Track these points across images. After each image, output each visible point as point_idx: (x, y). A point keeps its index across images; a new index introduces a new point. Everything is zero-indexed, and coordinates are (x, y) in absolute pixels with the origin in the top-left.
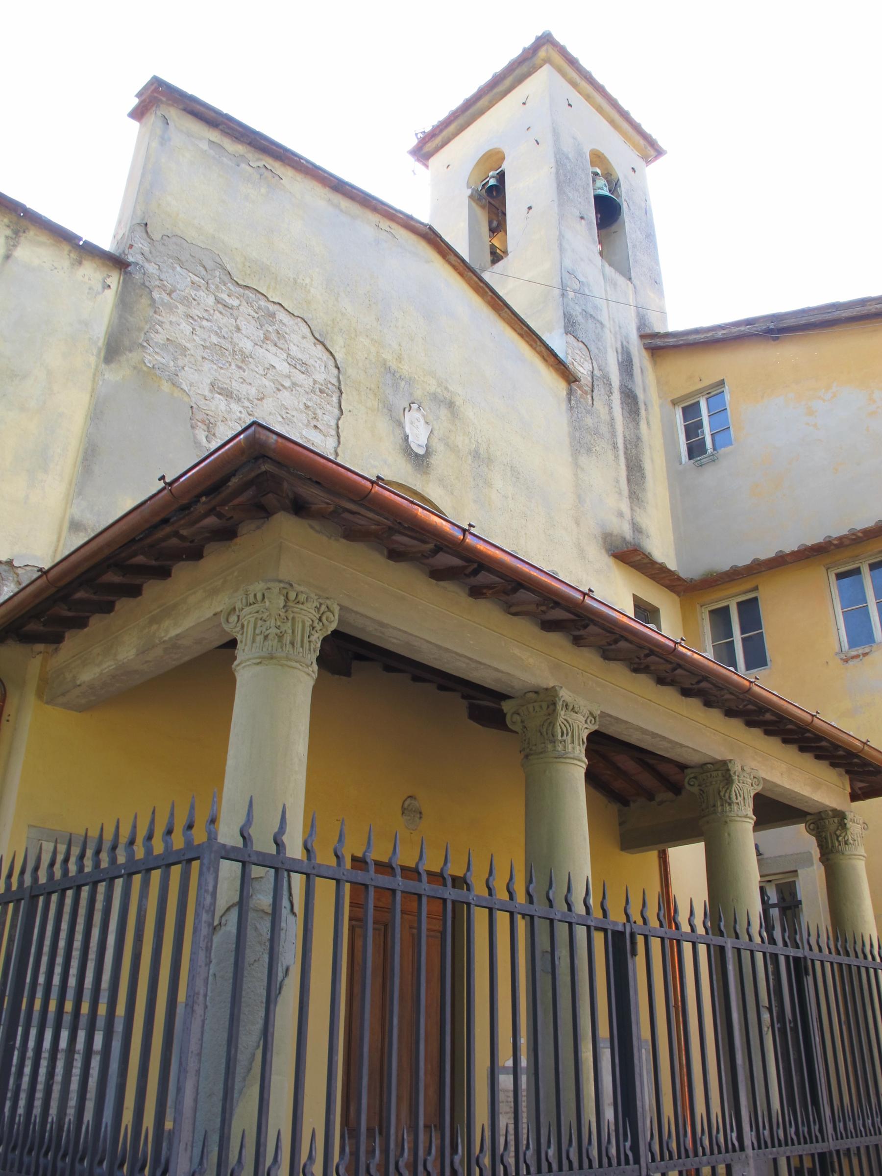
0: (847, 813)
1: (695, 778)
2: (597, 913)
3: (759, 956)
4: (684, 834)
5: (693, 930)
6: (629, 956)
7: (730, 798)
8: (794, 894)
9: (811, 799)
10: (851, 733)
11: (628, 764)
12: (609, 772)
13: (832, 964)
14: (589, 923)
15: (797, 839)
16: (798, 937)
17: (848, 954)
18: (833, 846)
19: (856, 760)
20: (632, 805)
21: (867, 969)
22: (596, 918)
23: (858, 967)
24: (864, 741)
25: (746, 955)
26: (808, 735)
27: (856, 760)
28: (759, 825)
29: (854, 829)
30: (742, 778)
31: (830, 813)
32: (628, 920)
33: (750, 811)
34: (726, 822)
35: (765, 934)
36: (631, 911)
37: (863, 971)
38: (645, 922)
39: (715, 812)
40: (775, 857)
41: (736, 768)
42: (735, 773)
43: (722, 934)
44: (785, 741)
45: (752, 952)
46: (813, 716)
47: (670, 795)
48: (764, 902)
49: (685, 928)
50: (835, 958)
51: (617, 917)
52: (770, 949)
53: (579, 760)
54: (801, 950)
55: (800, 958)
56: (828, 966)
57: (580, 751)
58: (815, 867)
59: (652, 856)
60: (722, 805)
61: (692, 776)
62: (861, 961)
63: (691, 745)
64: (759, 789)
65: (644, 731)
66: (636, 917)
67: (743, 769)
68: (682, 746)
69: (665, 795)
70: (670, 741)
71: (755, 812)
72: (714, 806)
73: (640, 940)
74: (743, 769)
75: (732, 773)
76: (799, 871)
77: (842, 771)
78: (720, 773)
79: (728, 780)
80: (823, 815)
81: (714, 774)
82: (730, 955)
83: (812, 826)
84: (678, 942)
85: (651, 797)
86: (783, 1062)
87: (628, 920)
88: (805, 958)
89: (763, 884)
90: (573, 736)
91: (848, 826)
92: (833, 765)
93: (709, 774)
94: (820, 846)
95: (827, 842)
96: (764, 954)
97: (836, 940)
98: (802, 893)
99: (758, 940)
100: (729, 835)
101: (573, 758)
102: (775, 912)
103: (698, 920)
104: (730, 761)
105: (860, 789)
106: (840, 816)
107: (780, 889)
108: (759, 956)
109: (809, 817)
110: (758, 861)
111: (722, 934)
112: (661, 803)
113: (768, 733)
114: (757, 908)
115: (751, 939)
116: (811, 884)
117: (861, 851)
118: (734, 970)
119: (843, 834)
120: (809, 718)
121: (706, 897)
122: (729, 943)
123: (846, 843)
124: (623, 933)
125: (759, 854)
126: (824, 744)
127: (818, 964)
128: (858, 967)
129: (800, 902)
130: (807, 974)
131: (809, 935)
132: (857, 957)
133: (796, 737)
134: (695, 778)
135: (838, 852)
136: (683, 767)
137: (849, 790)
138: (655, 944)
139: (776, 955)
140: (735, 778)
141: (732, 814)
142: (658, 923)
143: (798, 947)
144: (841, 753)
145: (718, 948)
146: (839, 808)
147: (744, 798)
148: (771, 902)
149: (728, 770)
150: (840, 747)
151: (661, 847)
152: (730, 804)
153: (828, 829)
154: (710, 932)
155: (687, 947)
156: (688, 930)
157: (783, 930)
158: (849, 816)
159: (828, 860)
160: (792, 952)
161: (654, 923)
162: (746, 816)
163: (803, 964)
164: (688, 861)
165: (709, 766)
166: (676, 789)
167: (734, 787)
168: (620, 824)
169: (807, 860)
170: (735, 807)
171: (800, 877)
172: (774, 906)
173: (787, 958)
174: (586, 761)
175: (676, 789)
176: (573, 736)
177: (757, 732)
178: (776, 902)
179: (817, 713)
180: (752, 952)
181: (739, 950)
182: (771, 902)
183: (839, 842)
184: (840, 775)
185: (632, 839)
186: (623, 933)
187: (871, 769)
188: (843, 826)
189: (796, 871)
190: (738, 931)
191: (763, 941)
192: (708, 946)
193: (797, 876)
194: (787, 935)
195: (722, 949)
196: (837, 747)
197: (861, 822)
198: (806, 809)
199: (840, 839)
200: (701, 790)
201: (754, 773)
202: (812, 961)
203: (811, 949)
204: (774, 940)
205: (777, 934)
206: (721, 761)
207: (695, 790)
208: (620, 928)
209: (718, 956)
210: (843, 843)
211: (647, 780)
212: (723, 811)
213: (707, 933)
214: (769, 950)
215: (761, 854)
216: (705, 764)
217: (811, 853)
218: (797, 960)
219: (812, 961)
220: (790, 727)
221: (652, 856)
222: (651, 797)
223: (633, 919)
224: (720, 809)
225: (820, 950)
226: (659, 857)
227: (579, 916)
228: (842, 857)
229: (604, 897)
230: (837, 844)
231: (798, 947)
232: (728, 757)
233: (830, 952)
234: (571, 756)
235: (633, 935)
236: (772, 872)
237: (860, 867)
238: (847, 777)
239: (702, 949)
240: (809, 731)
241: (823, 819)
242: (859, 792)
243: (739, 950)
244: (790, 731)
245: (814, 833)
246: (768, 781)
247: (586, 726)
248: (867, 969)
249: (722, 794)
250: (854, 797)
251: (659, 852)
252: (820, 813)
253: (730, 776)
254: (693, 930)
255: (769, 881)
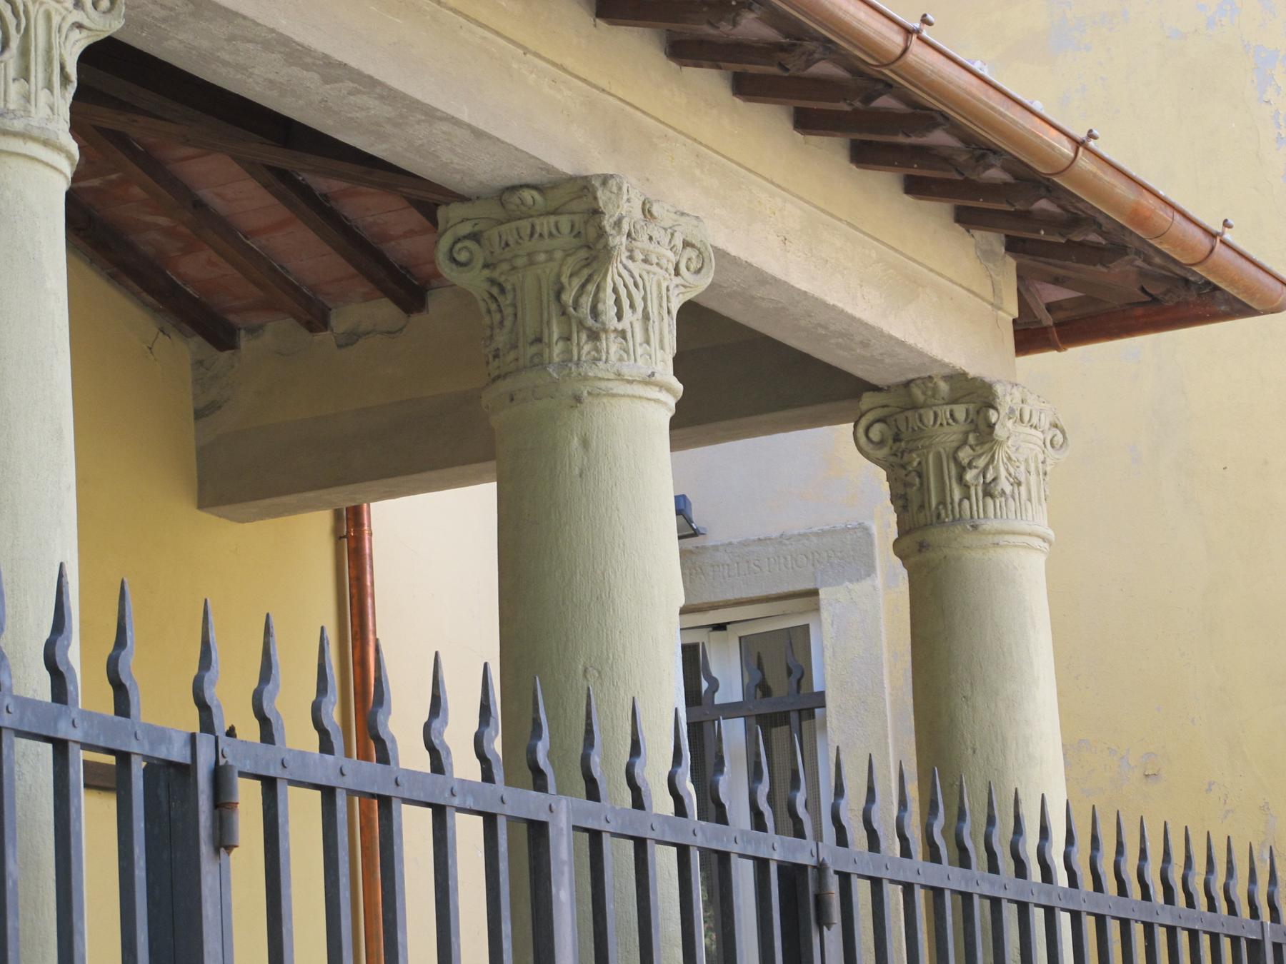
0: (999, 389)
1: (475, 237)
2: (91, 693)
3: (664, 862)
4: (425, 448)
5: (438, 765)
6: (205, 849)
7: (595, 313)
8: (799, 672)
9: (880, 334)
10: (1038, 106)
11: (228, 183)
12: (163, 221)
13: (908, 889)
14: (63, 731)
15: (822, 476)
16: (800, 798)
17: (963, 860)
18: (942, 502)
19: (1043, 204)
20: (244, 341)
21: (1023, 908)
22: (87, 715)
23: (996, 903)
24: (1081, 134)
25: (619, 857)
26: (884, 102)
27: (1043, 204)
28: (691, 423)
29: (1019, 443)
30: (642, 243)
31: (944, 387)
32: (207, 724)
33: (664, 366)
34: (578, 399)
35: (688, 788)
36: (216, 693)
37: (1010, 915)
38: (267, 734)
39: (539, 363)
40: (745, 544)
41: (622, 207)
42: (618, 223)
43: (539, 780)
44: (806, 122)
45: (640, 845)
46: (908, 32)
47: (385, 311)
48: (693, 696)
49: (411, 756)
50: (921, 871)
51: (165, 717)
52: (703, 835)
53: (46, 143)
54: (809, 842)
55: (803, 868)
56: (894, 896)
57: (53, 109)
58: (879, 580)
59: (313, 530)
60: (568, 339)
61: (466, 228)
62: (1005, 884)
63: (465, 117)
64: (697, 286)
65: (296, 53)
66: (234, 709)
67: (647, 212)
68: (431, 114)
69: (368, 312)
70: (391, 96)
71: (681, 366)
72: (539, 340)
73: (248, 796)
74: (647, 212)
75: (607, 223)
76: (821, 592)
77: (995, 241)
78: (564, 221)
79: (593, 250)
80: (917, 392)
81: (545, 224)
82: (565, 853)
83: (875, 433)
84: (385, 802)
85: (314, 316)
86: (706, 879)
87: (207, 724)
88: (821, 868)
89: (692, 638)
90: (24, 52)
91: (999, 432)
92: (967, 218)
93: (525, 225)
94: (901, 500)
95: (924, 488)
96: (683, 851)
97: (930, 809)
98: (829, 669)
99: (662, 803)
100: (585, 443)
101: (24, 136)
102: (733, 733)
103: (459, 733)
104: (605, 180)
105: (1050, 307)
106: (977, 397)
107: (755, 654)
108: (664, 862)
109: (868, 400)
110: (684, 554)
111: (539, 780)
112: (351, 338)
113: (745, 87)
114: (663, 702)
115: (638, 803)
116: (862, 642)
117: (1037, 519)
118: (578, 901)
119: (981, 463)
120: (894, 40)
121: (492, 653)
122: (564, 814)
123: (988, 493)
124: (185, 771)
125: (688, 531)
126: (939, 138)
127: (862, 891)
128: (996, 903)
129: (820, 699)
130: (823, 920)
131: (839, 791)
132: (993, 868)
133: (844, 107)
134: (475, 237)
135: (958, 520)
136: (428, 198)
137: (1012, 309)
138: (302, 810)
139: (724, 858)
140: (619, 241)
141: (600, 370)
142: (315, 736)
143: (800, 834)
144: (995, 174)
145: (524, 827)
146: (972, 372)
147: (646, 317)
148: (719, 699)
149: (596, 212)
150: (996, 151)
151: (344, 497)
152: (594, 336)
153: (932, 447)
154: (498, 773)
155: (415, 826)
156: (422, 763)
157: (755, 775)
158: (1007, 398)
159: (922, 547)
160: (779, 848)
161: (299, 735)
162: (649, 380)
163: (812, 888)
164: (436, 552)
165: (527, 195)
166: (409, 289)
167: (615, 275)
168: (199, 414)
169: (850, 555)
170: (612, 346)
171: (825, 614)
172: (730, 710)
173: (761, 865)
174: (73, 147)
175: (409, 289)
176: (24, 52)
177: (708, 82)
178: (737, 697)
179: (925, 20)
180: (640, 845)
181: (595, 837)
182: (719, 699)
183: (966, 487)
184: (986, 255)
185: (235, 476)
186: (185, 771)
187: (1093, 237)
188: (982, 432)
189: (814, 593)
190: (597, 772)
191: (680, 810)
192: (490, 821)
193: (816, 609)
194: (763, 789)
195: (537, 831)
196: (983, 151)
197: (1045, 423)
198: (859, 371)
199: (969, 476)
200: (493, 282)
201: (685, 229)
202: (845, 878)
203: (842, 840)
204: (720, 807)
205: (733, 786)
206: (572, 179)
207: (473, 280)
208: (178, 753)
209: (524, 855)
210: (976, 492)
211: (304, 253)
212: (567, 359)
213: (488, 776)
214: (700, 841)
215: (696, 533)
216: (514, 189)
217: (866, 531)
218: (792, 875)
219: (845, 878)
220: (824, 68)
221: (313, 530)
222: (314, 316)
223: (222, 722)
224: (557, 349)
225: (874, 842)
226: (338, 537)
227: (24, 703)
228: (970, 539)
229: (121, 641)
230: (957, 495)
231: (800, 834)
232: (597, 165)
233: (906, 852)
234: (18, 125)
235: (220, 777)
236: (731, 596)
237: (1026, 570)
238: (1011, 263)
239: (468, 833)
240: (889, 86)
241: (915, 407)
242: (1048, 320)
243: (595, 837)
244: (823, 86)
245: (882, 453)
246: (735, 261)
247: (77, 16)
248: (1023, 908)
249: (568, 298)
250: (1030, 337)
251: (337, 515)
252: (907, 384)
253: (601, 233)
254: (438, 765)
255: (721, 627)
